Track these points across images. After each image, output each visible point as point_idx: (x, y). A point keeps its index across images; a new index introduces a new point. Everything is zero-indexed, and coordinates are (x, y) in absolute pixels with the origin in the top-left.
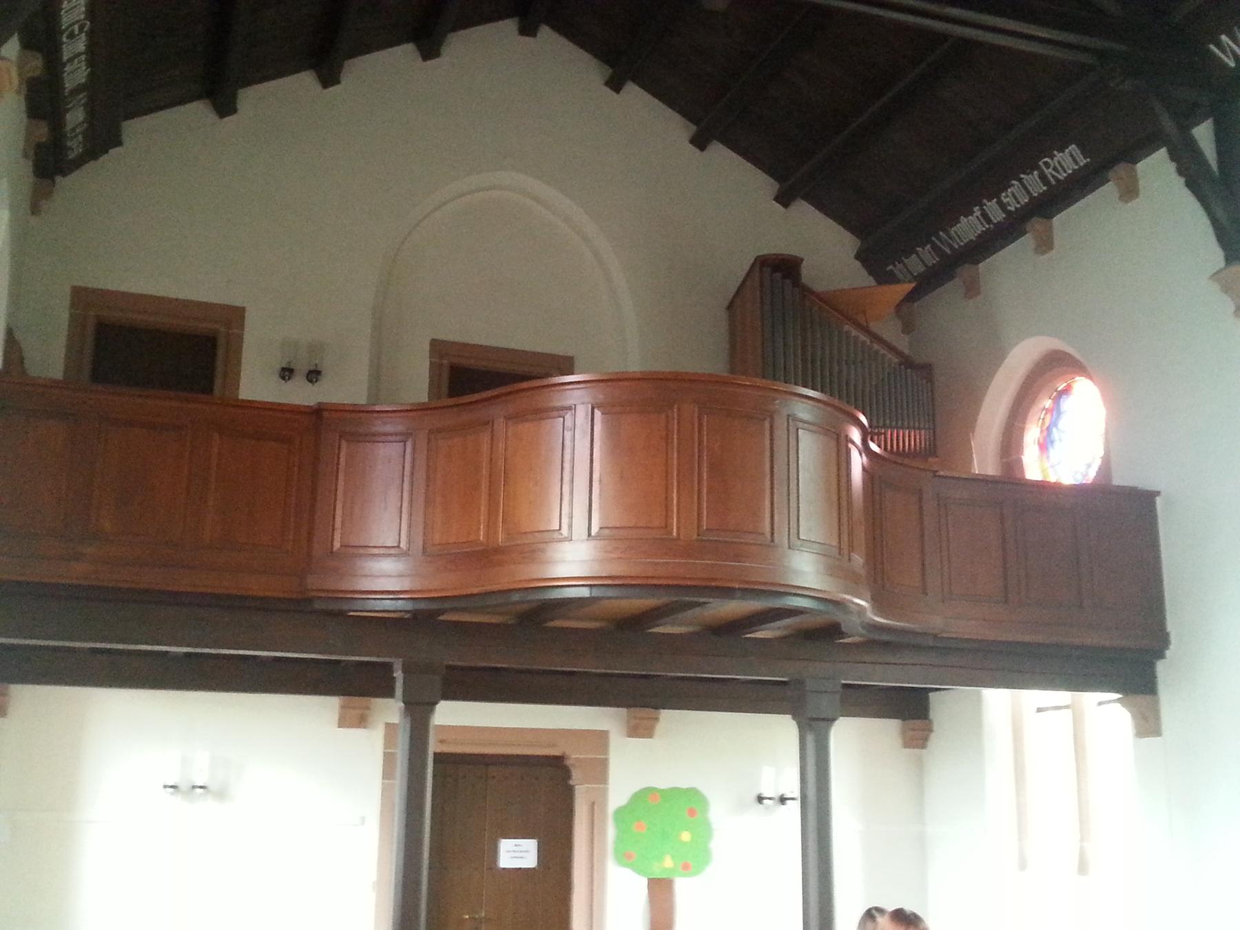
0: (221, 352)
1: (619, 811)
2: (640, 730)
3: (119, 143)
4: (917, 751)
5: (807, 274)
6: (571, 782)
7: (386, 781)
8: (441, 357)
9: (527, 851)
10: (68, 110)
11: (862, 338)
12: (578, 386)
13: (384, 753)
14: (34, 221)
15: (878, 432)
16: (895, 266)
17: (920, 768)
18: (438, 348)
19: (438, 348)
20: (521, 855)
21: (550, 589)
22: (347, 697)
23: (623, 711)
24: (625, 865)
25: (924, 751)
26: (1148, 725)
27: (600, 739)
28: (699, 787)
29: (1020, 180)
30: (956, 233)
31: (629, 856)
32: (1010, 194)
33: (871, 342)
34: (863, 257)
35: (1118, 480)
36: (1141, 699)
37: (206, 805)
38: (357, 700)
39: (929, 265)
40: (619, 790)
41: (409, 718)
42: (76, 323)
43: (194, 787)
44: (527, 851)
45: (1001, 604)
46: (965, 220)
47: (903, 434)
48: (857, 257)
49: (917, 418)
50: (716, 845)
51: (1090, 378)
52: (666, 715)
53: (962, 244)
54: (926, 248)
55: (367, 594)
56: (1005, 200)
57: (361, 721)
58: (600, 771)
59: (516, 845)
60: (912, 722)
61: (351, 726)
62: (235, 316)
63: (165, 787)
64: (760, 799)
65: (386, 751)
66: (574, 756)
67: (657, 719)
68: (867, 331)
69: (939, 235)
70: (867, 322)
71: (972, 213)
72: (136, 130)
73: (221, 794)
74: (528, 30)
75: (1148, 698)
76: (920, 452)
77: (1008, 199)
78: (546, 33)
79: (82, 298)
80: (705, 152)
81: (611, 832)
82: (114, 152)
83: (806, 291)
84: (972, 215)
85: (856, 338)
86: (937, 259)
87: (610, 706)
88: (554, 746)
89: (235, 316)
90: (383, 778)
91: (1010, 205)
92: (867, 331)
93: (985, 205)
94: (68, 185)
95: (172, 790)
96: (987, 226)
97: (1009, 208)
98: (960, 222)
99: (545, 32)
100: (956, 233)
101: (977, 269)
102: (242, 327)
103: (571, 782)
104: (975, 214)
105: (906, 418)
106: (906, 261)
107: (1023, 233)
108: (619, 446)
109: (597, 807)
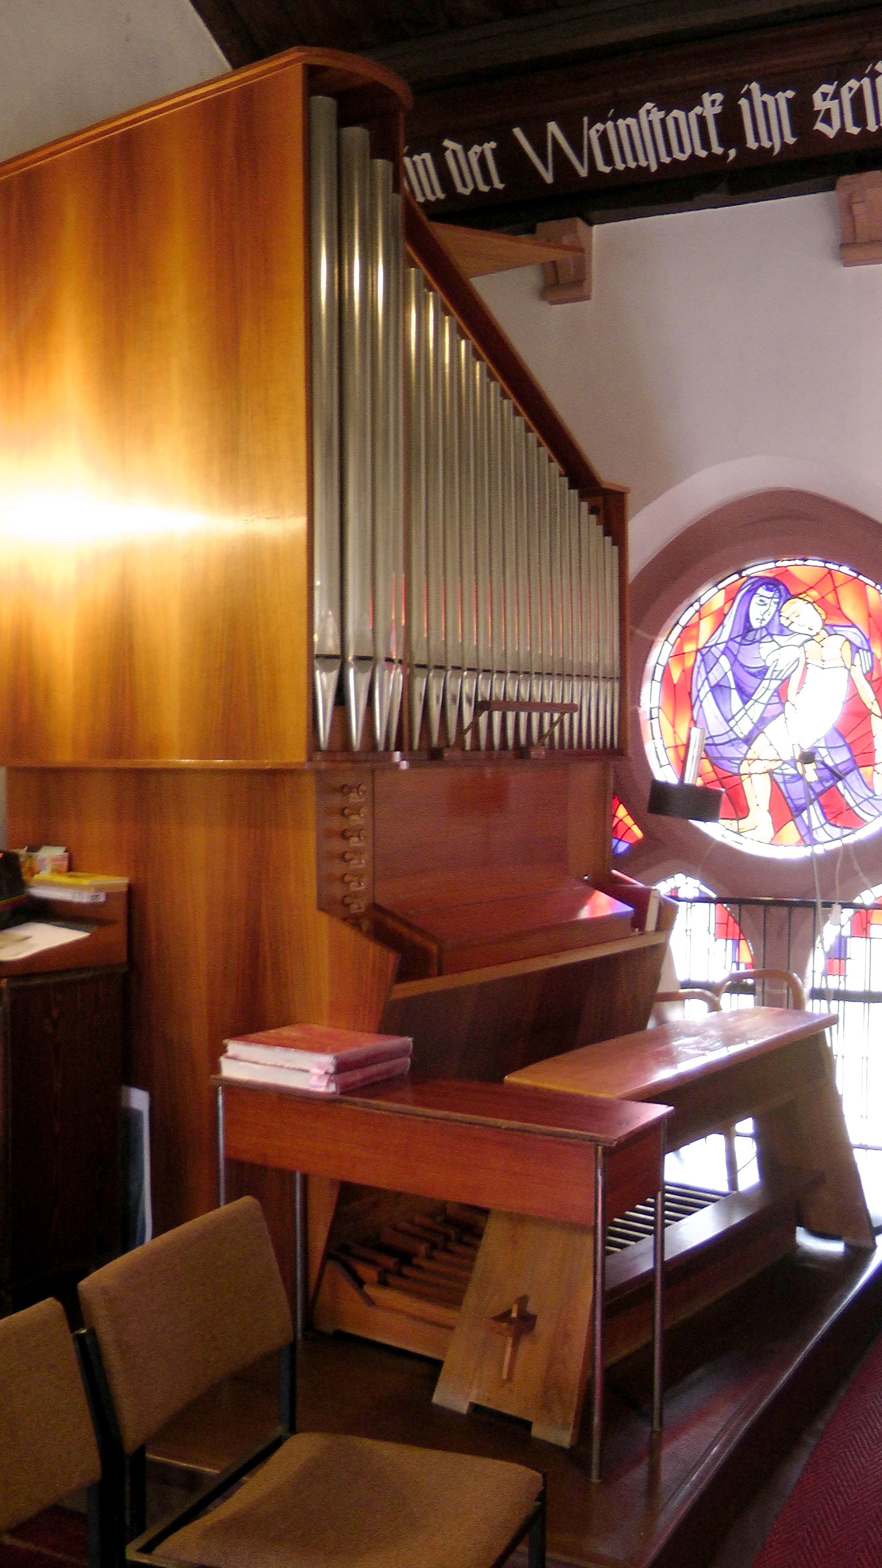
21: (713, 630)
30: (603, 138)
32: (846, 96)
35: (704, 1139)
39: (460, 189)
45: (304, 1105)
46: (657, 115)
51: (853, 915)
56: (819, 104)
70: (738, 652)
71: (689, 102)
77: (834, 105)
86: (498, 185)
91: (827, 119)
93: (748, 95)
96: (718, 150)
97: (820, 126)
100: (603, 138)
104: (698, 110)
107: (831, 187)
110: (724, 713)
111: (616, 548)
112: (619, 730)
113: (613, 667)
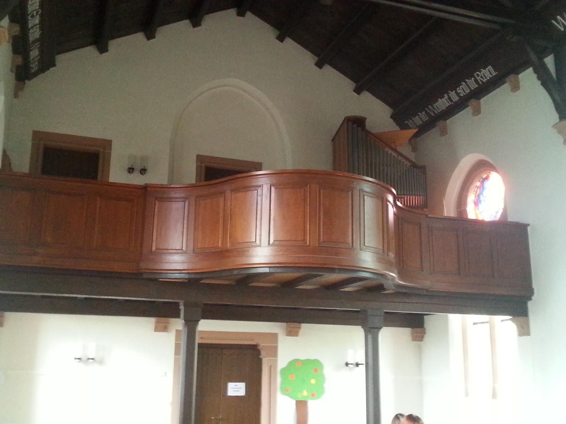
0: (101, 161)
1: (283, 370)
2: (292, 333)
3: (54, 65)
4: (418, 342)
5: (369, 125)
6: (261, 357)
7: (176, 356)
8: (201, 163)
9: (240, 388)
10: (31, 50)
11: (394, 154)
12: (264, 176)
13: (175, 343)
14: (15, 101)
15: (401, 197)
16: (408, 121)
17: (420, 350)
18: (200, 159)
19: (200, 159)
20: (238, 390)
22: (158, 318)
23: (284, 324)
24: (285, 395)
25: (422, 342)
26: (524, 330)
27: (274, 337)
28: (319, 359)
29: (466, 82)
30: (436, 106)
31: (287, 390)
32: (461, 89)
33: (398, 156)
34: (394, 117)
35: (510, 219)
36: (521, 319)
37: (94, 367)
38: (163, 319)
39: (424, 121)
40: (283, 360)
41: (187, 328)
42: (35, 147)
43: (88, 359)
44: (240, 388)
46: (441, 100)
47: (412, 198)
48: (391, 117)
49: (418, 191)
50: (327, 385)
51: (498, 172)
52: (304, 326)
53: (439, 111)
54: (423, 113)
55: (167, 271)
56: (459, 91)
57: (165, 329)
58: (274, 351)
59: (235, 385)
60: (416, 329)
61: (160, 331)
62: (107, 144)
63: (75, 359)
64: (347, 364)
65: (176, 342)
66: (262, 345)
67: (300, 328)
68: (396, 151)
69: (429, 107)
71: (443, 97)
72: (62, 59)
73: (101, 362)
74: (241, 14)
75: (524, 318)
76: (420, 206)
77: (460, 91)
78: (249, 15)
79: (37, 136)
80: (322, 69)
81: (279, 379)
82: (52, 69)
83: (368, 133)
84: (444, 98)
85: (391, 154)
86: (428, 118)
87: (279, 322)
88: (253, 340)
89: (107, 144)
90: (175, 355)
91: (461, 94)
92: (396, 151)
93: (450, 93)
94: (31, 84)
95: (79, 360)
96: (451, 103)
97: (461, 95)
98: (438, 101)
99: (249, 14)
100: (436, 106)
101: (446, 123)
102: (110, 149)
103: (261, 357)
104: (445, 98)
105: (413, 191)
106: (413, 119)
107: (467, 106)
108: (282, 204)
109: (272, 368)
110: (258, 199)
111: (411, 120)
112: (198, 408)
113: (183, 190)
